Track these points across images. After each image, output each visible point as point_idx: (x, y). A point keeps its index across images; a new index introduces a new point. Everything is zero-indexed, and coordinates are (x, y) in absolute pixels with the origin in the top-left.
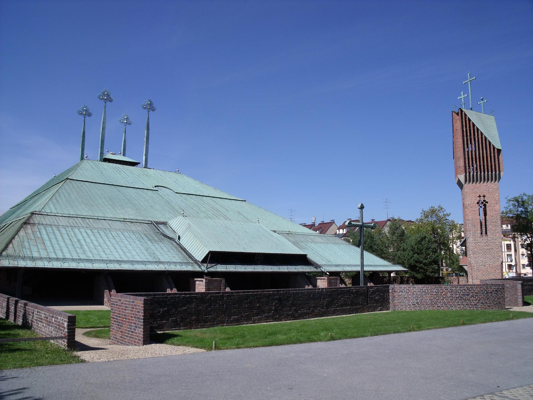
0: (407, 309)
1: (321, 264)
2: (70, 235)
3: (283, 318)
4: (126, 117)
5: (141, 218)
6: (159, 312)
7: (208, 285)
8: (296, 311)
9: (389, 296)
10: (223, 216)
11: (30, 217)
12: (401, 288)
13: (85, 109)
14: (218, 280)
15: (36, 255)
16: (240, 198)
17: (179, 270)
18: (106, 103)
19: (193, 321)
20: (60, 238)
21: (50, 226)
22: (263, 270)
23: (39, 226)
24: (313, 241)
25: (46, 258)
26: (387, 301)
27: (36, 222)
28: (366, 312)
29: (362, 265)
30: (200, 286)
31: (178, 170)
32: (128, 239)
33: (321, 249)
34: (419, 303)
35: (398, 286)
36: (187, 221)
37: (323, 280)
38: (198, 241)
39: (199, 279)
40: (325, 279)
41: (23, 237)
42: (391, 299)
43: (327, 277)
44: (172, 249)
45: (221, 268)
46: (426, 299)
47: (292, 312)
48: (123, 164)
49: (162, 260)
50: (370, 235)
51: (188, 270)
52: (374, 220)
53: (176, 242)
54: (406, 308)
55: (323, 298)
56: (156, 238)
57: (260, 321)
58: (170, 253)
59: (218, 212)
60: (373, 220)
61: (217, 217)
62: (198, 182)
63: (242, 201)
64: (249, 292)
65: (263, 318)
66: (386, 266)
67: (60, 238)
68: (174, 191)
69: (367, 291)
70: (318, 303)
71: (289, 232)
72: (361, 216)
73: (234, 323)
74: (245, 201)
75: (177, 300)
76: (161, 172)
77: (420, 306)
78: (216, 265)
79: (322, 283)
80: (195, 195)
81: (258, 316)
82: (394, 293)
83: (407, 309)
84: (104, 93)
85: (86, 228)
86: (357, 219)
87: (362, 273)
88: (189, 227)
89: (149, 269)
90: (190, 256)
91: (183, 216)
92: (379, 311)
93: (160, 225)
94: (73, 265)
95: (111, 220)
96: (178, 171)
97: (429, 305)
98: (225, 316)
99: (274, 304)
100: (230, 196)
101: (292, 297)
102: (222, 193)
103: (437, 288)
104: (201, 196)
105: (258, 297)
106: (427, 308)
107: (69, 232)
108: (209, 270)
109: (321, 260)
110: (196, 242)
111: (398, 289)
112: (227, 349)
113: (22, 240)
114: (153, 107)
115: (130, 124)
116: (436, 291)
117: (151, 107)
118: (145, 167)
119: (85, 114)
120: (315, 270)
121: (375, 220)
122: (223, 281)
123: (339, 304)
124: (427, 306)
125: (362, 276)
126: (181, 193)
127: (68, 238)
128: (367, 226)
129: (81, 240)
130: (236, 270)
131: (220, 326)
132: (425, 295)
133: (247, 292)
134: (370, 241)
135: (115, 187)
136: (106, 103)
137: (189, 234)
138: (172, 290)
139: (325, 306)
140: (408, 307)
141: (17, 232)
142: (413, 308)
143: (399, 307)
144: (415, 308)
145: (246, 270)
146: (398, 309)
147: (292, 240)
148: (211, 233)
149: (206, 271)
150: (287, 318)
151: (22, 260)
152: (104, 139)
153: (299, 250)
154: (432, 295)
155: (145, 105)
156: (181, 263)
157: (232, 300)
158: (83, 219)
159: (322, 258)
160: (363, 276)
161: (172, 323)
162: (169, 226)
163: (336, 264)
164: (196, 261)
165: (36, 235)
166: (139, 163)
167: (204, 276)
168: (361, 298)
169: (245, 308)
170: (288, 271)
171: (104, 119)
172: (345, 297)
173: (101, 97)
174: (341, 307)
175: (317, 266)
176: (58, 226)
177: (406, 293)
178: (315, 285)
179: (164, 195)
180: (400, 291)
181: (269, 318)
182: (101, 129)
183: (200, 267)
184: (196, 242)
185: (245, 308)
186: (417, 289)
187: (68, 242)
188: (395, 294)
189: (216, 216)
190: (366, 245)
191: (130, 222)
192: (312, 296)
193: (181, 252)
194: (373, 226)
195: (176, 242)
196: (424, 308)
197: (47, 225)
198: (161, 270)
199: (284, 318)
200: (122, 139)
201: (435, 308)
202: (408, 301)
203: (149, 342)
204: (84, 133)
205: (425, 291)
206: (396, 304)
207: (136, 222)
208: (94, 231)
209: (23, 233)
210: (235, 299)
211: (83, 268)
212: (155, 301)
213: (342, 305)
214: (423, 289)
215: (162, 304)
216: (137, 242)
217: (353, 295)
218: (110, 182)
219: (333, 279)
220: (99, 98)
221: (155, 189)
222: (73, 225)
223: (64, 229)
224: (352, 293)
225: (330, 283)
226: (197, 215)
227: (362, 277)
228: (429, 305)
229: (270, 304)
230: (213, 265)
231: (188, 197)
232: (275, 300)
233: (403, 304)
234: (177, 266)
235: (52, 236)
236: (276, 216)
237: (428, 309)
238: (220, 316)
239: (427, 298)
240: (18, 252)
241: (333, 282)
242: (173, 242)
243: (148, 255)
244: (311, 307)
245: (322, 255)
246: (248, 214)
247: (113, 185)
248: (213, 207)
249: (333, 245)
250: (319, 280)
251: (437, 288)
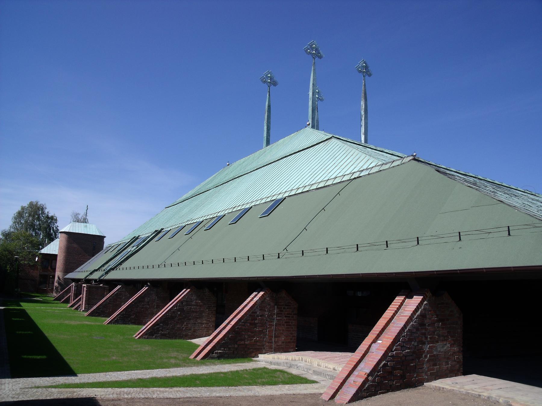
13: (269, 75)
117: (366, 71)
155: (360, 68)
173: (309, 51)
185: (438, 327)
220: (306, 51)
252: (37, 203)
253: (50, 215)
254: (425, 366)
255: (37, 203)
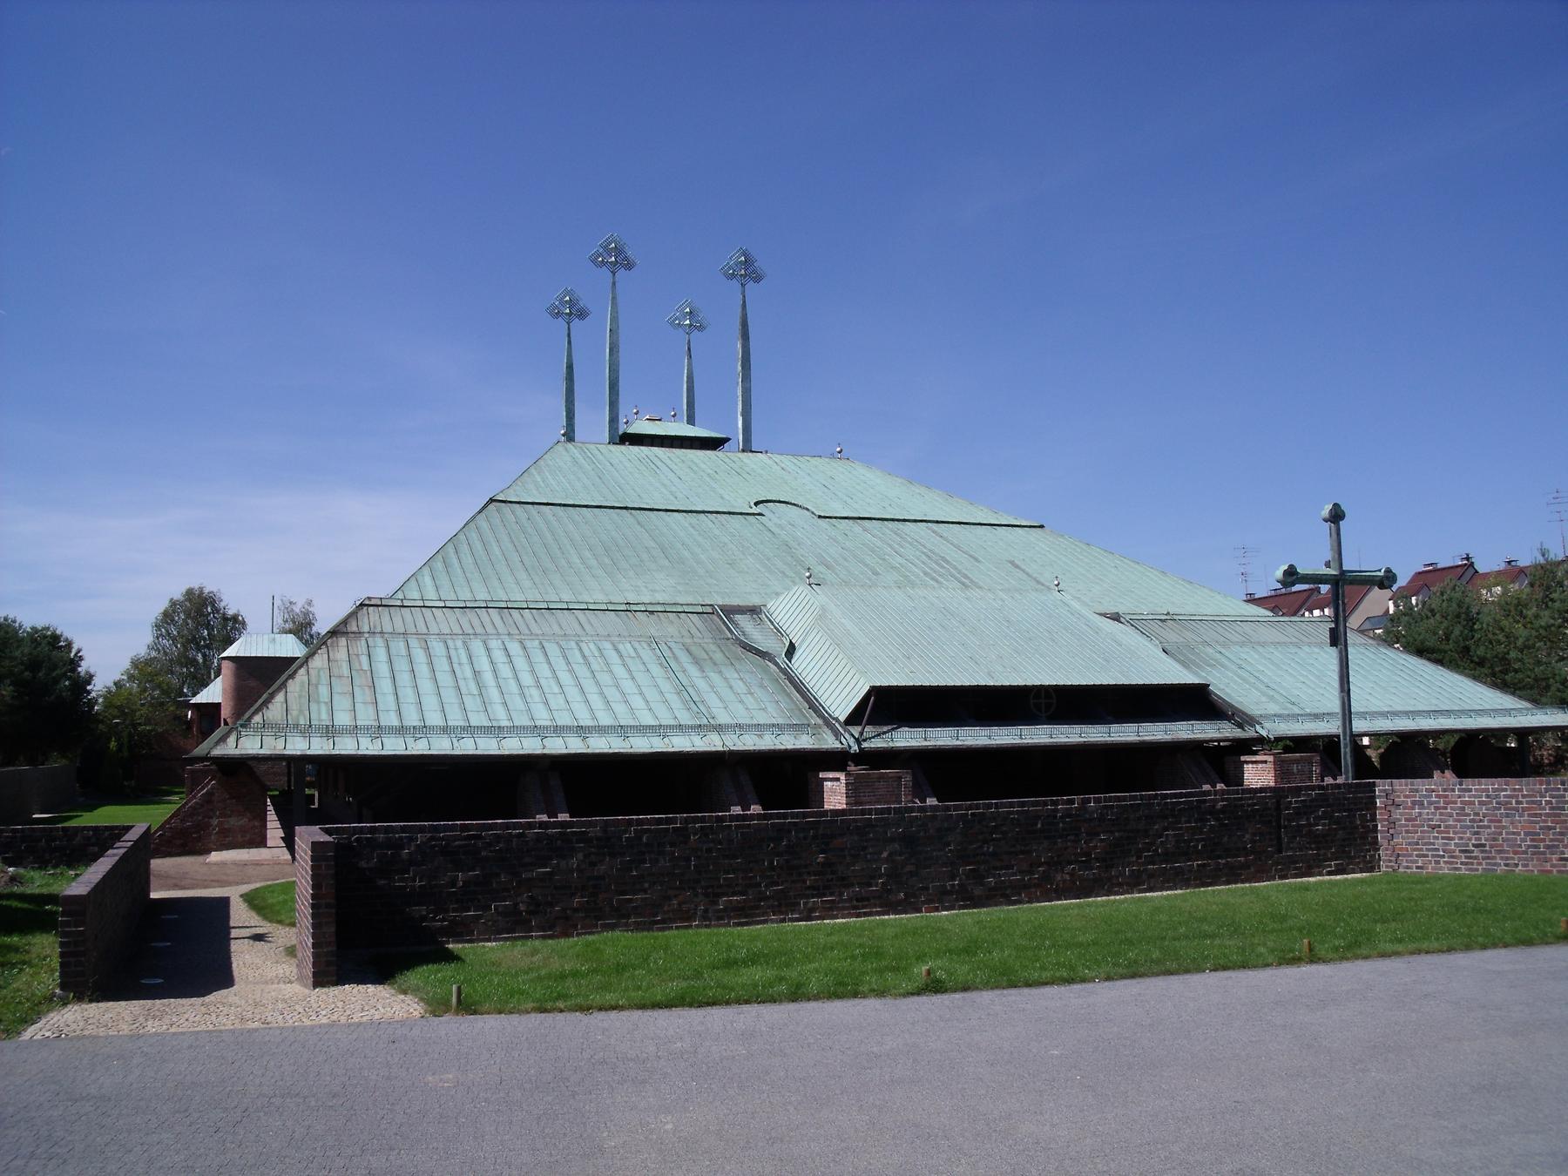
0: (1441, 869)
1: (1262, 712)
2: (455, 660)
3: (924, 903)
4: (688, 310)
5: (690, 600)
6: (453, 884)
7: (853, 791)
8: (977, 876)
9: (1374, 818)
10: (956, 579)
11: (353, 614)
12: (1417, 791)
14: (890, 775)
15: (343, 719)
16: (1025, 520)
17: (768, 748)
18: (614, 273)
19: (576, 910)
20: (422, 669)
21: (402, 636)
22: (1052, 740)
23: (370, 640)
24: (1247, 642)
25: (463, 729)
26: (1364, 837)
27: (366, 629)
28: (1274, 879)
29: (1347, 713)
30: (835, 793)
31: (838, 449)
32: (629, 662)
33: (1273, 663)
34: (1484, 845)
35: (1406, 785)
36: (820, 597)
37: (1260, 766)
38: (841, 656)
39: (831, 775)
40: (1266, 762)
41: (319, 672)
42: (1382, 832)
43: (1272, 757)
44: (762, 686)
45: (907, 738)
46: (1514, 833)
47: (960, 880)
48: (672, 446)
49: (723, 718)
50: (1464, 610)
51: (799, 747)
52: (1513, 563)
53: (776, 664)
54: (1437, 862)
55: (1086, 833)
56: (718, 656)
57: (830, 911)
58: (753, 697)
59: (943, 567)
60: (1509, 562)
61: (937, 581)
62: (900, 480)
63: (1031, 527)
64: (785, 816)
65: (845, 901)
66: (1507, 712)
67: (422, 669)
68: (813, 513)
69: (1278, 803)
70: (1066, 849)
71: (1168, 614)
72: (1335, 544)
73: (730, 918)
74: (1042, 527)
75: (514, 843)
76: (786, 461)
77: (1488, 858)
78: (893, 729)
79: (1258, 774)
80: (878, 519)
81: (825, 896)
82: (1392, 809)
83: (1441, 869)
84: (606, 248)
85: (507, 637)
86: (1456, 564)
87: (1345, 739)
88: (823, 615)
89: (673, 750)
90: (814, 705)
91: (810, 585)
92: (1330, 873)
93: (738, 617)
94: (441, 746)
95: (607, 610)
96: (839, 452)
97: (1525, 852)
98: (696, 896)
99: (885, 855)
100: (995, 515)
101: (958, 831)
102: (970, 507)
103: (1553, 790)
104: (898, 520)
105: (821, 832)
106: (1517, 865)
107: (453, 653)
108: (865, 745)
109: (1264, 699)
110: (837, 661)
111: (1406, 796)
112: (500, 1013)
113: (314, 681)
114: (754, 272)
115: (701, 328)
116: (1554, 800)
117: (748, 271)
118: (743, 451)
119: (570, 314)
120: (1238, 733)
121: (1518, 564)
122: (907, 779)
123: (1157, 850)
124: (1520, 859)
125: (1348, 750)
126: (836, 518)
127: (447, 668)
128: (1358, 578)
129: (407, 669)
130: (959, 743)
131: (677, 928)
132: (1507, 815)
133: (778, 816)
134: (1462, 632)
135: (631, 514)
136: (614, 273)
137: (817, 639)
138: (746, 807)
139: (1097, 859)
140: (1446, 862)
141: (307, 658)
142: (1462, 863)
143: (1412, 861)
144: (1472, 864)
145: (994, 742)
146: (1407, 867)
147: (1175, 640)
148: (891, 630)
149: (855, 748)
150: (940, 901)
151: (298, 734)
152: (617, 378)
153: (1185, 672)
154: (1536, 815)
156: (778, 728)
157: (720, 843)
158: (506, 610)
159: (1271, 693)
160: (1351, 752)
161: (500, 918)
162: (766, 616)
163: (1316, 711)
164: (828, 721)
165: (357, 664)
166: (727, 440)
167: (849, 763)
168: (1250, 831)
169: (773, 868)
170: (1138, 738)
171: (614, 319)
172: (1181, 829)
174: (1166, 862)
175: (1239, 718)
176: (424, 639)
177: (1436, 808)
178: (1239, 780)
179: (779, 526)
180: (1414, 803)
181: (866, 903)
182: (608, 350)
183: (837, 735)
184: (837, 661)
186: (1475, 796)
187: (445, 679)
188: (1397, 814)
189: (933, 579)
190: (1451, 646)
191: (646, 611)
192: (1039, 826)
193: (788, 695)
194: (1382, 577)
195: (776, 664)
196: (1506, 865)
197: (394, 635)
198: (709, 749)
199: (929, 901)
200: (683, 373)
201: (1549, 864)
202: (1443, 838)
203: (334, 978)
204: (570, 367)
205: (1507, 803)
206: (1401, 849)
207: (665, 612)
208: (528, 644)
209: (323, 660)
210: (733, 840)
211: (470, 753)
212: (437, 849)
213: (1168, 857)
214: (1497, 796)
215: (463, 857)
216: (656, 670)
217: (1217, 819)
218: (619, 501)
219: (1297, 761)
220: (594, 261)
221: (755, 510)
222: (471, 631)
223: (441, 644)
224: (1212, 811)
225: (1282, 770)
226: (870, 580)
227: (1345, 753)
228: (1525, 852)
229: (871, 854)
230: (885, 729)
231: (856, 527)
232: (892, 840)
233: (1428, 850)
234: (766, 737)
235: (402, 665)
236: (1137, 566)
237: (1520, 868)
238: (676, 896)
239: (1516, 827)
240: (295, 713)
241: (1295, 771)
242: (770, 664)
243: (681, 706)
244: (1041, 865)
245: (1270, 685)
246: (1042, 565)
247: (626, 508)
248: (930, 550)
249: (1316, 650)
250: (1250, 766)
251: (1553, 790)
252: (201, 589)
253: (231, 612)
254: (213, 837)
255: (201, 589)
